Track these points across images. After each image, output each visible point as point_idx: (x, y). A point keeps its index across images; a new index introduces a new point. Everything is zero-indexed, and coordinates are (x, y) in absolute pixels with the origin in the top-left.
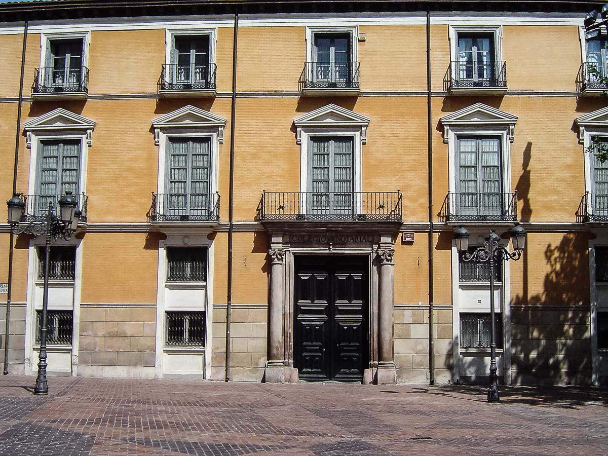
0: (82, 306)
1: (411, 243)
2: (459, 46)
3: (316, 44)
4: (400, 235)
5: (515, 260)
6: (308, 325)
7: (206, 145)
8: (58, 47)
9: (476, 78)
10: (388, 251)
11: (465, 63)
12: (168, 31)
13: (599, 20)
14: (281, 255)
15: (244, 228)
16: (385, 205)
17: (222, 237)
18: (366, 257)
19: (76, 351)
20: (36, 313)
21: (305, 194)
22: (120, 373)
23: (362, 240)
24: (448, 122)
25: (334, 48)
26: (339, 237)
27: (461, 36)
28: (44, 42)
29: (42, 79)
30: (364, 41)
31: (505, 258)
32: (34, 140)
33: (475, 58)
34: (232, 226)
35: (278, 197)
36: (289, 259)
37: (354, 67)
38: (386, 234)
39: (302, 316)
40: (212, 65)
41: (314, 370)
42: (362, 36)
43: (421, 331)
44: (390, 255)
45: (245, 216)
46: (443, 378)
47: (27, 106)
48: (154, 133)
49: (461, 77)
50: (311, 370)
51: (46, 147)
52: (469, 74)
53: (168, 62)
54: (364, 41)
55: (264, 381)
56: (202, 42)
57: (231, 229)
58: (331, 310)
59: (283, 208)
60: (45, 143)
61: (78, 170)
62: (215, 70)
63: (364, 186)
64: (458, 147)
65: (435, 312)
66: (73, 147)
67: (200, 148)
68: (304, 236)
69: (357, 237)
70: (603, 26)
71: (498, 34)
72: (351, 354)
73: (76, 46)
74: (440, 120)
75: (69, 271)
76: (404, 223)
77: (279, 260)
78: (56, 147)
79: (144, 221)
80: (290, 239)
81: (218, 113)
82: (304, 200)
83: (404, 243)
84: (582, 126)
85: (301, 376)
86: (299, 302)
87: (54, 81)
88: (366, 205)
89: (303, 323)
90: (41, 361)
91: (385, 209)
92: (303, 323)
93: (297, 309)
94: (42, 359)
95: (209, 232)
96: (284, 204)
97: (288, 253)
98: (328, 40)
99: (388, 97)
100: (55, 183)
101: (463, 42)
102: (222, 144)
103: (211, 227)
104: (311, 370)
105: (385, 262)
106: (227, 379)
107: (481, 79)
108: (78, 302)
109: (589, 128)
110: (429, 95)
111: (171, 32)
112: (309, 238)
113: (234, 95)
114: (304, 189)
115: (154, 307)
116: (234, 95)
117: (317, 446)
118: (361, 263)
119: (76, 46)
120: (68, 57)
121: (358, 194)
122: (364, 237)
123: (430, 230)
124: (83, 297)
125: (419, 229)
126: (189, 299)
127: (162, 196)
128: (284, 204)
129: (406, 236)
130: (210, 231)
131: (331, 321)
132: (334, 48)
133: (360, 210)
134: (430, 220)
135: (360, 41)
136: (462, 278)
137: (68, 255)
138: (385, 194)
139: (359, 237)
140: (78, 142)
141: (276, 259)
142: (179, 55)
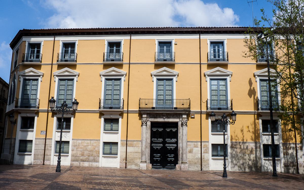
1: (194, 118)
2: (211, 46)
5: (233, 124)
6: (155, 148)
9: (217, 58)
13: (263, 37)
16: (184, 104)
19: (33, 156)
20: (56, 142)
22: (86, 164)
27: (212, 43)
28: (61, 44)
30: (177, 44)
31: (229, 124)
33: (217, 51)
35: (181, 101)
36: (149, 123)
38: (185, 114)
40: (122, 53)
41: (158, 164)
43: (197, 150)
45: (134, 107)
46: (247, 170)
48: (152, 77)
49: (212, 58)
52: (215, 57)
53: (26, 52)
54: (177, 44)
56: (118, 44)
57: (128, 112)
58: (164, 143)
59: (147, 104)
60: (158, 80)
61: (120, 90)
64: (210, 83)
65: (202, 143)
68: (154, 115)
69: (174, 115)
70: (264, 39)
71: (225, 43)
72: (171, 159)
73: (73, 45)
74: (204, 73)
75: (68, 127)
79: (97, 109)
81: (124, 71)
83: (191, 118)
84: (206, 75)
86: (166, 139)
87: (64, 58)
90: (58, 159)
93: (152, 142)
94: (59, 158)
97: (148, 121)
100: (217, 95)
103: (121, 111)
105: (184, 125)
107: (219, 58)
109: (259, 76)
110: (52, 64)
111: (107, 41)
113: (130, 63)
114: (155, 97)
115: (99, 140)
116: (52, 64)
118: (175, 125)
119: (73, 45)
120: (36, 49)
125: (197, 113)
130: (120, 113)
134: (48, 108)
135: (175, 44)
136: (212, 132)
137: (68, 121)
138: (145, 100)
141: (144, 123)
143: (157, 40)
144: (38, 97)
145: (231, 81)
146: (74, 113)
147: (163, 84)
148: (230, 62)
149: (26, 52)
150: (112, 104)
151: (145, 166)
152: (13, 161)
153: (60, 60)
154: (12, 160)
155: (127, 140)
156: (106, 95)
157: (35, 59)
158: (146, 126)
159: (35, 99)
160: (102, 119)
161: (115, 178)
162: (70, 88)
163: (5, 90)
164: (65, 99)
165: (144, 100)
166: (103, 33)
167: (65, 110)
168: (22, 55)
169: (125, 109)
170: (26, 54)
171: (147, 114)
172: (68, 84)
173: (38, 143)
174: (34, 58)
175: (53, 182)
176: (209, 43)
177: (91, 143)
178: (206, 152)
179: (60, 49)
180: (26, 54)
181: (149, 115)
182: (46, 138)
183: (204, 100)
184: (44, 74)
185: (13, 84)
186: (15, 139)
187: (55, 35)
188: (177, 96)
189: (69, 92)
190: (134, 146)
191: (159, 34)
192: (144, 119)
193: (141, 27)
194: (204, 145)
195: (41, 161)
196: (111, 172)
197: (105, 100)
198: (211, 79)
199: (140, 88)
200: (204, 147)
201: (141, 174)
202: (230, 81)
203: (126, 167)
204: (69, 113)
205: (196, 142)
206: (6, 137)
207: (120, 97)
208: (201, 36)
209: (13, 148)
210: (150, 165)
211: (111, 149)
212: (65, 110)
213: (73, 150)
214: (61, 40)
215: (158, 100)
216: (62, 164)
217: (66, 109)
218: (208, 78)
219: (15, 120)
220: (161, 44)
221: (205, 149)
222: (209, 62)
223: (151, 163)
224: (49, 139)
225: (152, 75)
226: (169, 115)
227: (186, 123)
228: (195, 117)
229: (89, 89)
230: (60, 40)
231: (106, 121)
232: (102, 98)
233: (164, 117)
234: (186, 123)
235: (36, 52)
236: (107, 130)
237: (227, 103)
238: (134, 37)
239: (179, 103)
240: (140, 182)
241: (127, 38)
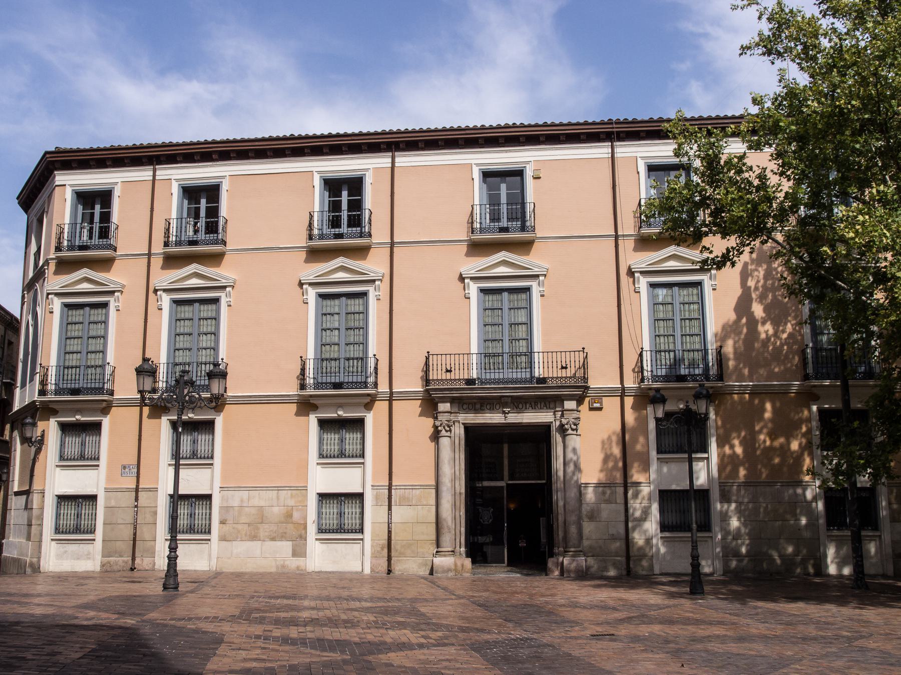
1: (600, 409)
3: (484, 181)
4: (587, 400)
7: (361, 300)
8: (191, 193)
12: (315, 174)
14: (449, 426)
15: (406, 396)
17: (381, 407)
18: (547, 427)
19: (99, 543)
21: (475, 356)
27: (487, 175)
28: (175, 189)
30: (539, 178)
32: (166, 300)
34: (391, 393)
36: (459, 431)
37: (529, 208)
38: (570, 398)
40: (367, 212)
42: (537, 173)
44: (575, 425)
45: (409, 381)
47: (157, 262)
48: (302, 288)
51: (325, 302)
55: (431, 573)
60: (484, 291)
62: (370, 216)
69: (536, 403)
77: (447, 431)
81: (374, 265)
82: (475, 362)
83: (591, 409)
90: (170, 552)
91: (568, 370)
94: (173, 549)
97: (457, 424)
98: (498, 179)
99: (275, 254)
103: (368, 395)
105: (570, 432)
106: (389, 572)
108: (217, 484)
114: (474, 349)
115: (305, 489)
116: (149, 255)
117: (390, 649)
118: (544, 431)
121: (536, 354)
124: (224, 477)
125: (609, 392)
126: (344, 479)
127: (312, 361)
130: (368, 400)
135: (535, 178)
138: (554, 354)
140: (105, 305)
143: (477, 165)
144: (110, 357)
145: (717, 287)
146: (218, 403)
147: (190, 316)
149: (67, 220)
150: (342, 374)
151: (453, 561)
152: (39, 561)
153: (173, 239)
154: (35, 560)
155: (137, 486)
156: (321, 345)
157: (96, 240)
159: (102, 367)
160: (313, 420)
161: (345, 605)
162: (96, 330)
163: (13, 340)
164: (195, 364)
165: (572, 353)
166: (306, 151)
167: (187, 398)
168: (54, 230)
169: (383, 387)
170: (66, 227)
171: (453, 401)
172: (92, 319)
173: (113, 503)
174: (91, 238)
175: (143, 621)
177: (278, 498)
179: (172, 206)
180: (66, 227)
181: (459, 403)
182: (137, 486)
184: (124, 286)
185: (31, 322)
186: (43, 493)
187: (158, 164)
189: (94, 345)
190: (414, 502)
191: (482, 146)
192: (443, 418)
193: (448, 127)
195: (125, 559)
196: (340, 584)
197: (321, 360)
198: (653, 286)
199: (429, 319)
201: (433, 590)
202: (714, 289)
203: (389, 572)
204: (200, 407)
206: (16, 489)
207: (366, 351)
208: (617, 150)
209: (39, 523)
210: (468, 562)
211: (341, 514)
212: (187, 398)
213: (223, 522)
214: (179, 175)
215: (487, 356)
216: (183, 564)
217: (189, 392)
218: (643, 283)
219: (39, 434)
220: (333, 185)
222: (478, 237)
223: (467, 556)
224: (149, 490)
225: (301, 284)
226: (520, 403)
227: (574, 427)
228: (604, 406)
229: (267, 329)
230: (173, 177)
231: (324, 424)
232: (311, 354)
233: (507, 410)
234: (574, 427)
235: (97, 218)
236: (327, 457)
237: (365, 367)
238: (405, 160)
239: (550, 363)
240: (423, 615)
241: (382, 161)
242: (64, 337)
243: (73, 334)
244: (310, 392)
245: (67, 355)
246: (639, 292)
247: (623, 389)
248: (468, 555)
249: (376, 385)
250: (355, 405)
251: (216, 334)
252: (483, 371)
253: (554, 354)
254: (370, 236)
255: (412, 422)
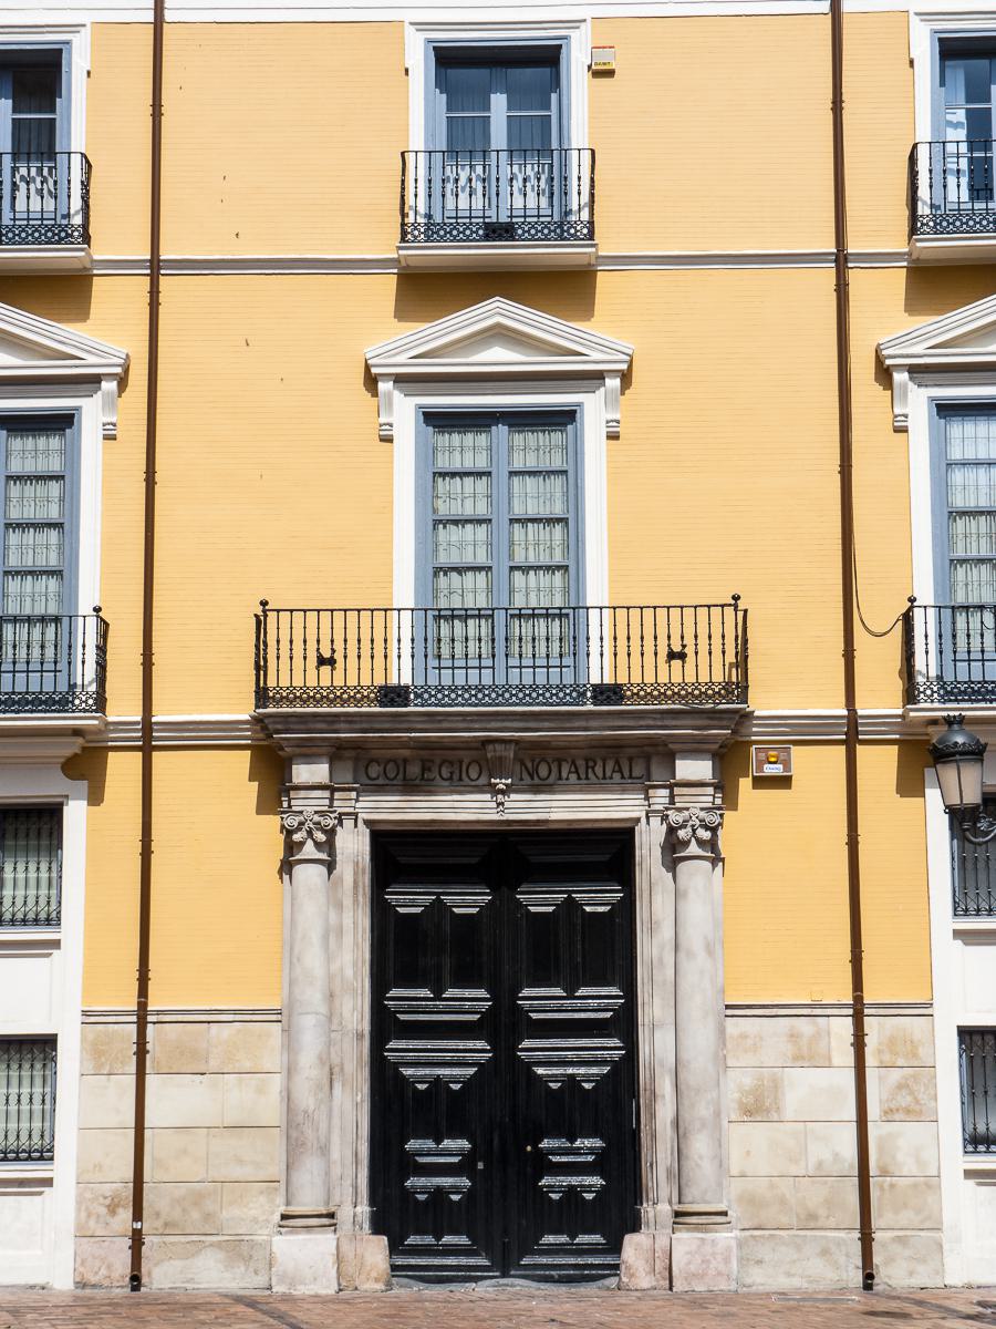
0: (729, 1012)
1: (784, 782)
2: (942, 83)
3: (442, 83)
6: (554, 1078)
10: (702, 809)
11: (964, 148)
12: (410, 31)
15: (202, 737)
16: (690, 651)
21: (406, 616)
23: (608, 774)
24: (908, 356)
25: (505, 96)
26: (529, 765)
29: (575, 182)
30: (610, 73)
34: (147, 725)
35: (339, 623)
36: (354, 845)
38: (694, 749)
39: (402, 1044)
40: (76, 160)
48: (375, 393)
49: (952, 196)
50: (433, 1241)
51: (444, 440)
54: (610, 73)
58: (504, 1025)
60: (437, 420)
63: (613, 581)
64: (939, 444)
66: (42, 442)
67: (530, 448)
68: (405, 761)
69: (590, 763)
76: (756, 714)
77: (701, 843)
78: (482, 439)
80: (355, 771)
81: (104, 333)
85: (400, 1261)
88: (622, 651)
89: (540, 1071)
92: (540, 1071)
93: (384, 1025)
95: (68, 752)
96: (333, 651)
97: (349, 823)
98: (484, 73)
101: (958, 73)
102: (113, 438)
103: (77, 732)
104: (433, 1241)
105: (694, 849)
106: (136, 1281)
111: (423, 36)
112: (424, 770)
113: (155, 267)
114: (404, 593)
118: (609, 853)
122: (617, 762)
123: (851, 733)
125: (810, 732)
128: (684, 646)
129: (762, 756)
130: (74, 746)
131: (506, 1073)
132: (505, 96)
133: (598, 671)
135: (598, 74)
136: (960, 909)
138: (312, 616)
139: (600, 763)
142: (13, 119)
143: (420, 26)
148: (607, 244)
158: (323, 870)
165: (298, 616)
168: (907, 1311)
169: (124, 708)
171: (336, 753)
176: (418, 59)
178: (908, 1111)
183: (878, 610)
188: (616, 577)
190: (214, 1064)
192: (309, 805)
194: (891, 1043)
200: (887, 1058)
203: (136, 1281)
205: (814, 1010)
207: (69, 594)
210: (376, 1251)
218: (917, 402)
221: (895, 1076)
222: (933, 245)
225: (371, 382)
226: (541, 764)
227: (705, 835)
228: (795, 772)
233: (501, 783)
242: (430, 517)
243: (456, 510)
244: (930, 707)
245: (442, 579)
246: (904, 430)
247: (852, 719)
248: (378, 1227)
249: (101, 702)
250: (36, 765)
251: (567, 522)
252: (433, 663)
253: (312, 616)
254: (86, 238)
255: (212, 796)
